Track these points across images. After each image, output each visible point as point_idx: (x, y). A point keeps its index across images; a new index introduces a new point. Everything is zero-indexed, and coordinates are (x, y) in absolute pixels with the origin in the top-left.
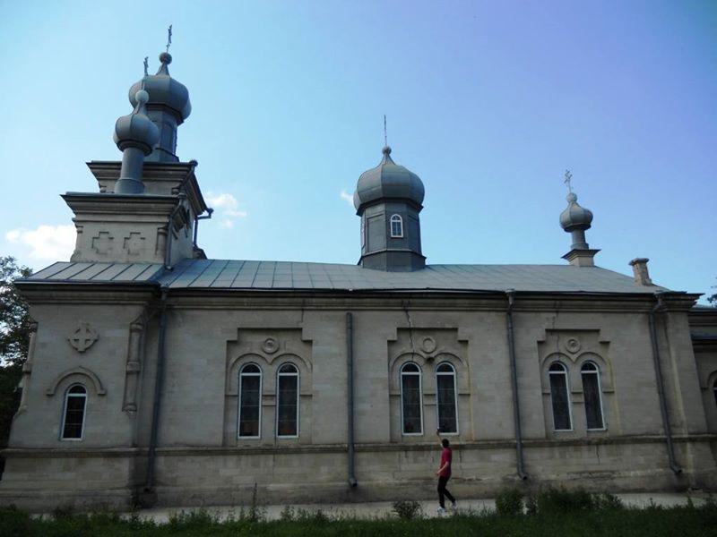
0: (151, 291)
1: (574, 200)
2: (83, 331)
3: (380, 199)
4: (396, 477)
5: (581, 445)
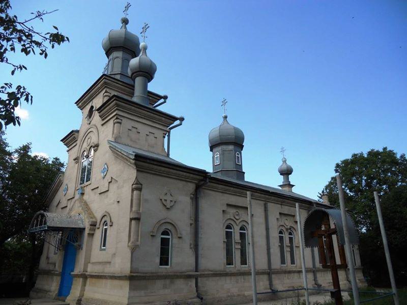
0: (203, 176)
1: (285, 161)
2: (169, 195)
3: (232, 143)
4: (284, 286)
5: (291, 273)
